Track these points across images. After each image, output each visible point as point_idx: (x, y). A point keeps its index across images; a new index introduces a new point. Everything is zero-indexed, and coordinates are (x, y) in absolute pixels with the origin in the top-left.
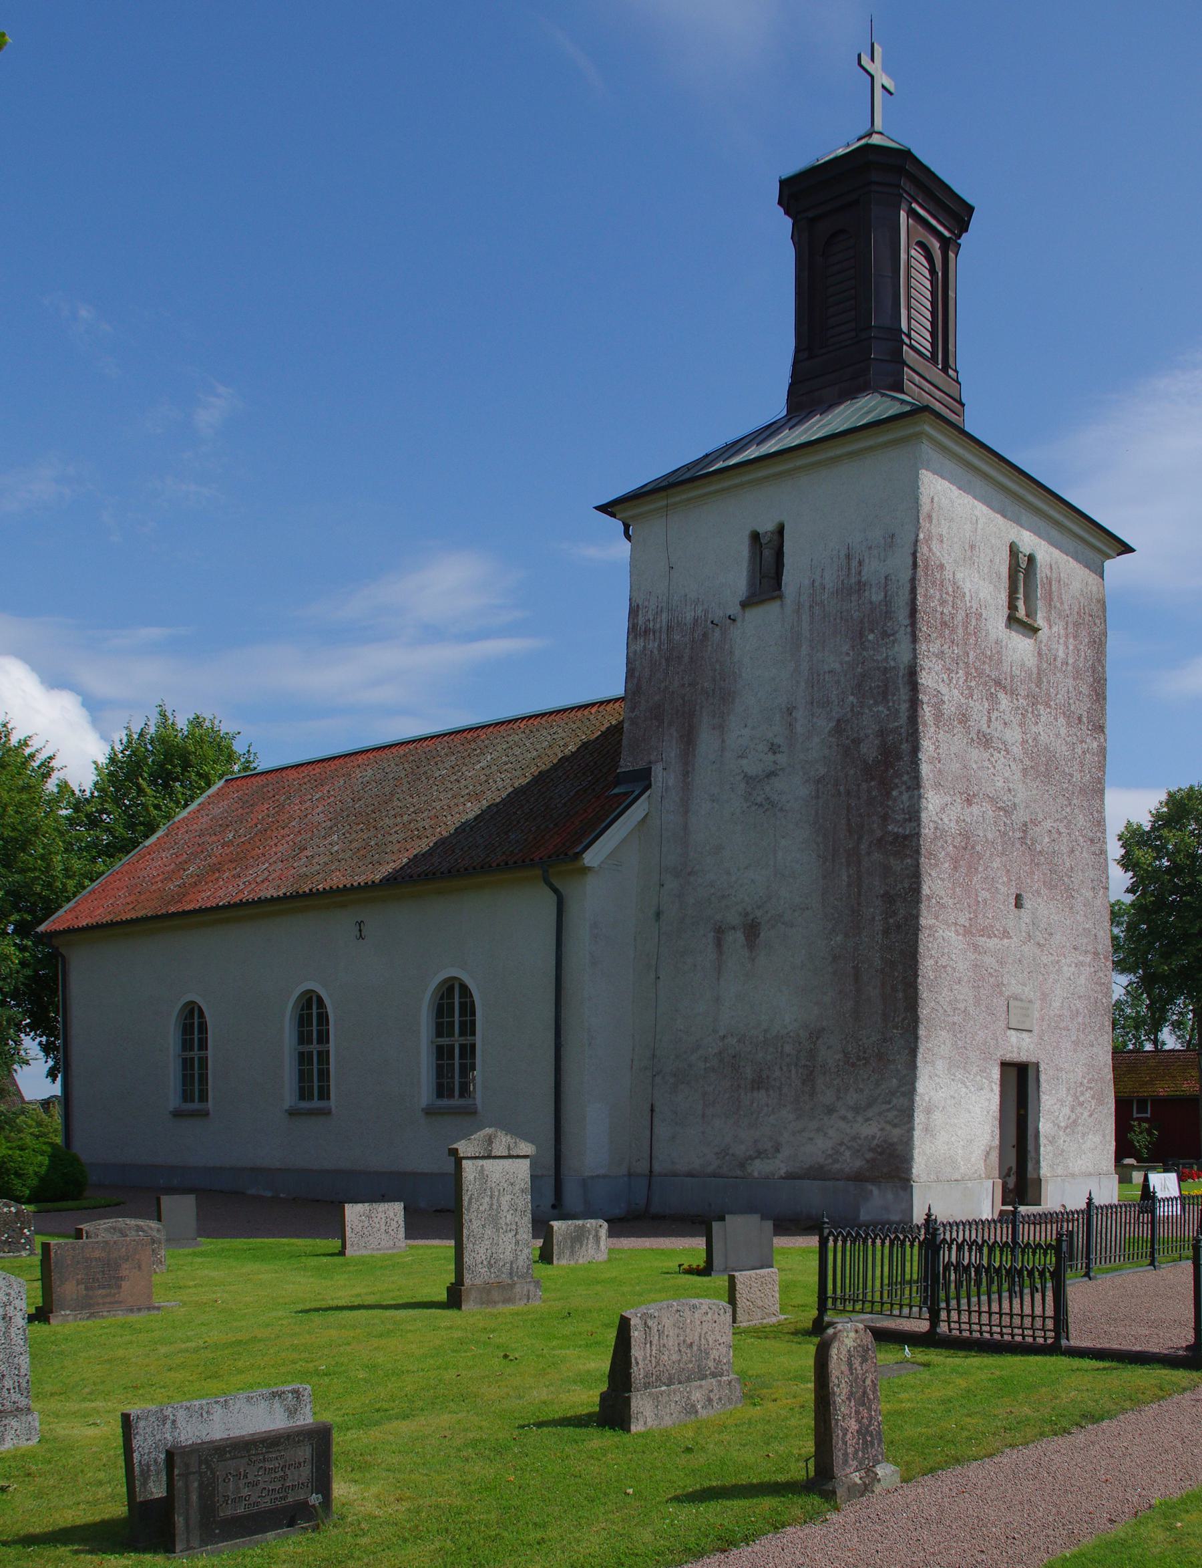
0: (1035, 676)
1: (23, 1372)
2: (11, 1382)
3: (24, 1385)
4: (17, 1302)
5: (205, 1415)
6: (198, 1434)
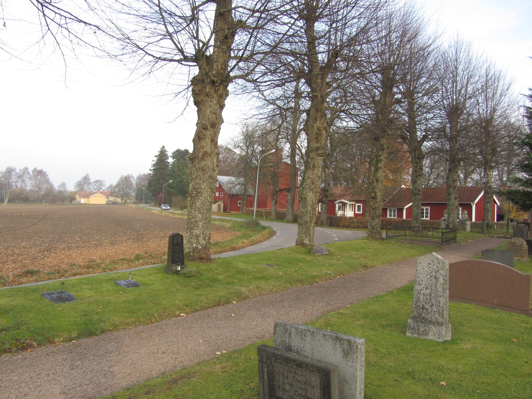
0: (489, 112)
1: (441, 305)
2: (436, 309)
3: (441, 311)
4: (441, 271)
5: (303, 336)
6: (299, 345)
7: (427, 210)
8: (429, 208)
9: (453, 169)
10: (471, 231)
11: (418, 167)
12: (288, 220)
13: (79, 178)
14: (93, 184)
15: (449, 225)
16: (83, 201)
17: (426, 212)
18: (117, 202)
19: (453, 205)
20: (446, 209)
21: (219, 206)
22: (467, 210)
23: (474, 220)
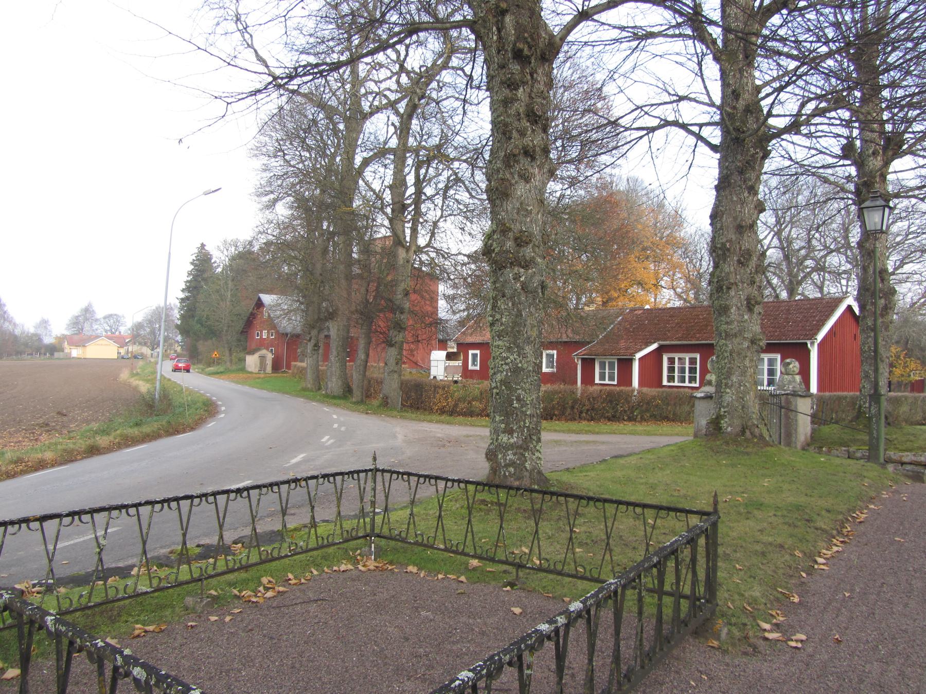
7: (693, 361)
8: (698, 356)
9: (735, 178)
10: (816, 442)
11: (520, 107)
12: (329, 392)
13: (76, 311)
14: (102, 321)
15: (724, 423)
16: (75, 353)
17: (690, 369)
18: (142, 354)
19: (741, 332)
20: (713, 354)
21: (263, 358)
22: (797, 359)
23: (814, 388)
